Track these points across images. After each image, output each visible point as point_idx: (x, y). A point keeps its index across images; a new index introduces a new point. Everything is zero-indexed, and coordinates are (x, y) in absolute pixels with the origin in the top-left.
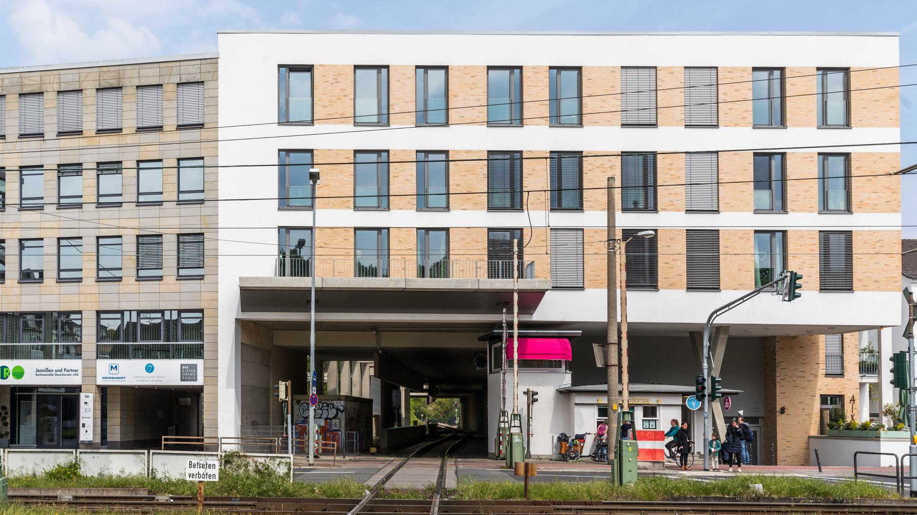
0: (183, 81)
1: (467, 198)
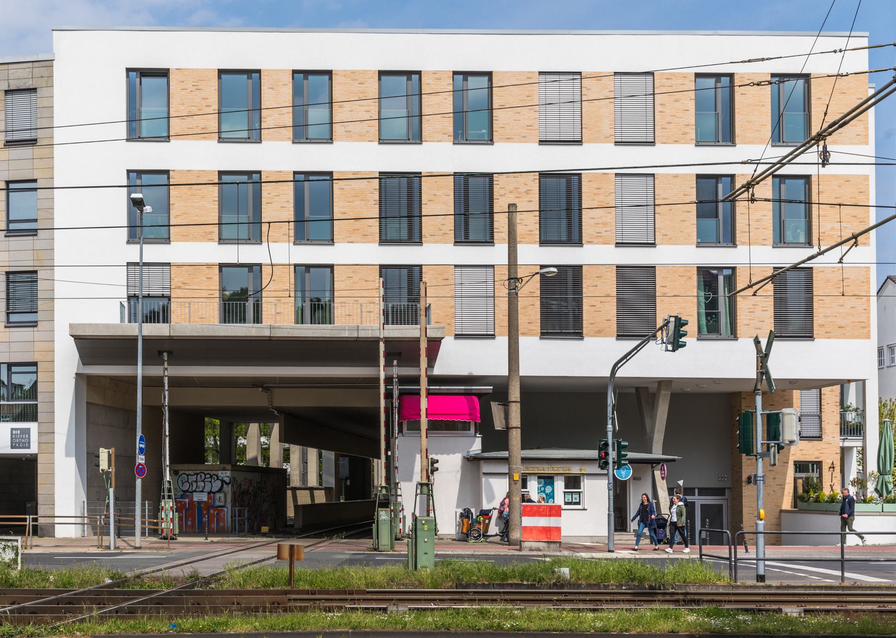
0: (12, 88)
1: (354, 228)
